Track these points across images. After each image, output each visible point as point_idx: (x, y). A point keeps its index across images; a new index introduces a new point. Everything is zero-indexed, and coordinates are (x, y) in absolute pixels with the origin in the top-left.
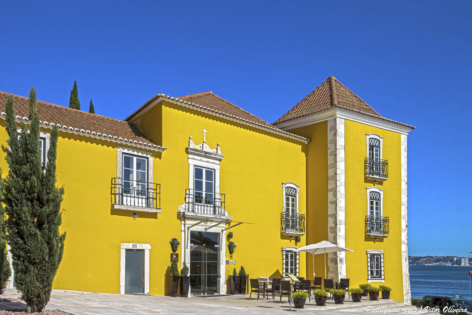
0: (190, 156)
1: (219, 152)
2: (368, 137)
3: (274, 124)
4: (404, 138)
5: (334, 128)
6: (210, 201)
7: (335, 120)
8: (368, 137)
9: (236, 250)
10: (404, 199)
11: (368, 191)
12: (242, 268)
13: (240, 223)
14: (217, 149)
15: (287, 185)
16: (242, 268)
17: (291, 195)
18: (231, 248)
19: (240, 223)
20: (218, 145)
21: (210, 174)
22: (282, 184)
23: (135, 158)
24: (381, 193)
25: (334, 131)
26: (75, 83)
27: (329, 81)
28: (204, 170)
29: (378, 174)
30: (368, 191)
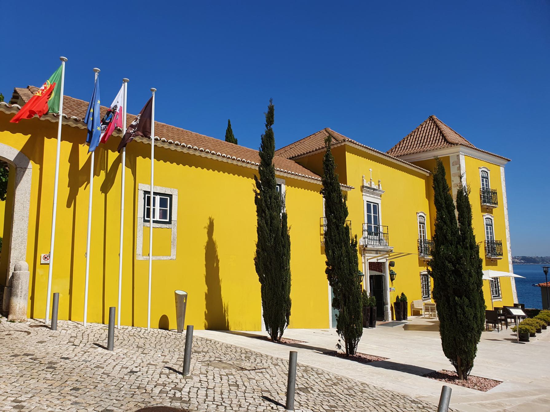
0: (364, 194)
1: (381, 188)
2: (480, 170)
3: (397, 156)
4: (502, 169)
5: (458, 163)
6: (377, 233)
7: (458, 156)
8: (480, 170)
9: (396, 278)
10: (507, 224)
11: (485, 217)
12: (403, 294)
13: (409, 254)
14: (379, 185)
15: (420, 214)
16: (403, 294)
17: (255, 191)
18: (392, 275)
19: (409, 254)
20: (379, 181)
21: (376, 207)
22: (417, 213)
23: (372, 204)
24: (492, 218)
25: (458, 166)
26: (229, 122)
27: (431, 119)
28: (372, 204)
29: (489, 202)
30: (485, 217)
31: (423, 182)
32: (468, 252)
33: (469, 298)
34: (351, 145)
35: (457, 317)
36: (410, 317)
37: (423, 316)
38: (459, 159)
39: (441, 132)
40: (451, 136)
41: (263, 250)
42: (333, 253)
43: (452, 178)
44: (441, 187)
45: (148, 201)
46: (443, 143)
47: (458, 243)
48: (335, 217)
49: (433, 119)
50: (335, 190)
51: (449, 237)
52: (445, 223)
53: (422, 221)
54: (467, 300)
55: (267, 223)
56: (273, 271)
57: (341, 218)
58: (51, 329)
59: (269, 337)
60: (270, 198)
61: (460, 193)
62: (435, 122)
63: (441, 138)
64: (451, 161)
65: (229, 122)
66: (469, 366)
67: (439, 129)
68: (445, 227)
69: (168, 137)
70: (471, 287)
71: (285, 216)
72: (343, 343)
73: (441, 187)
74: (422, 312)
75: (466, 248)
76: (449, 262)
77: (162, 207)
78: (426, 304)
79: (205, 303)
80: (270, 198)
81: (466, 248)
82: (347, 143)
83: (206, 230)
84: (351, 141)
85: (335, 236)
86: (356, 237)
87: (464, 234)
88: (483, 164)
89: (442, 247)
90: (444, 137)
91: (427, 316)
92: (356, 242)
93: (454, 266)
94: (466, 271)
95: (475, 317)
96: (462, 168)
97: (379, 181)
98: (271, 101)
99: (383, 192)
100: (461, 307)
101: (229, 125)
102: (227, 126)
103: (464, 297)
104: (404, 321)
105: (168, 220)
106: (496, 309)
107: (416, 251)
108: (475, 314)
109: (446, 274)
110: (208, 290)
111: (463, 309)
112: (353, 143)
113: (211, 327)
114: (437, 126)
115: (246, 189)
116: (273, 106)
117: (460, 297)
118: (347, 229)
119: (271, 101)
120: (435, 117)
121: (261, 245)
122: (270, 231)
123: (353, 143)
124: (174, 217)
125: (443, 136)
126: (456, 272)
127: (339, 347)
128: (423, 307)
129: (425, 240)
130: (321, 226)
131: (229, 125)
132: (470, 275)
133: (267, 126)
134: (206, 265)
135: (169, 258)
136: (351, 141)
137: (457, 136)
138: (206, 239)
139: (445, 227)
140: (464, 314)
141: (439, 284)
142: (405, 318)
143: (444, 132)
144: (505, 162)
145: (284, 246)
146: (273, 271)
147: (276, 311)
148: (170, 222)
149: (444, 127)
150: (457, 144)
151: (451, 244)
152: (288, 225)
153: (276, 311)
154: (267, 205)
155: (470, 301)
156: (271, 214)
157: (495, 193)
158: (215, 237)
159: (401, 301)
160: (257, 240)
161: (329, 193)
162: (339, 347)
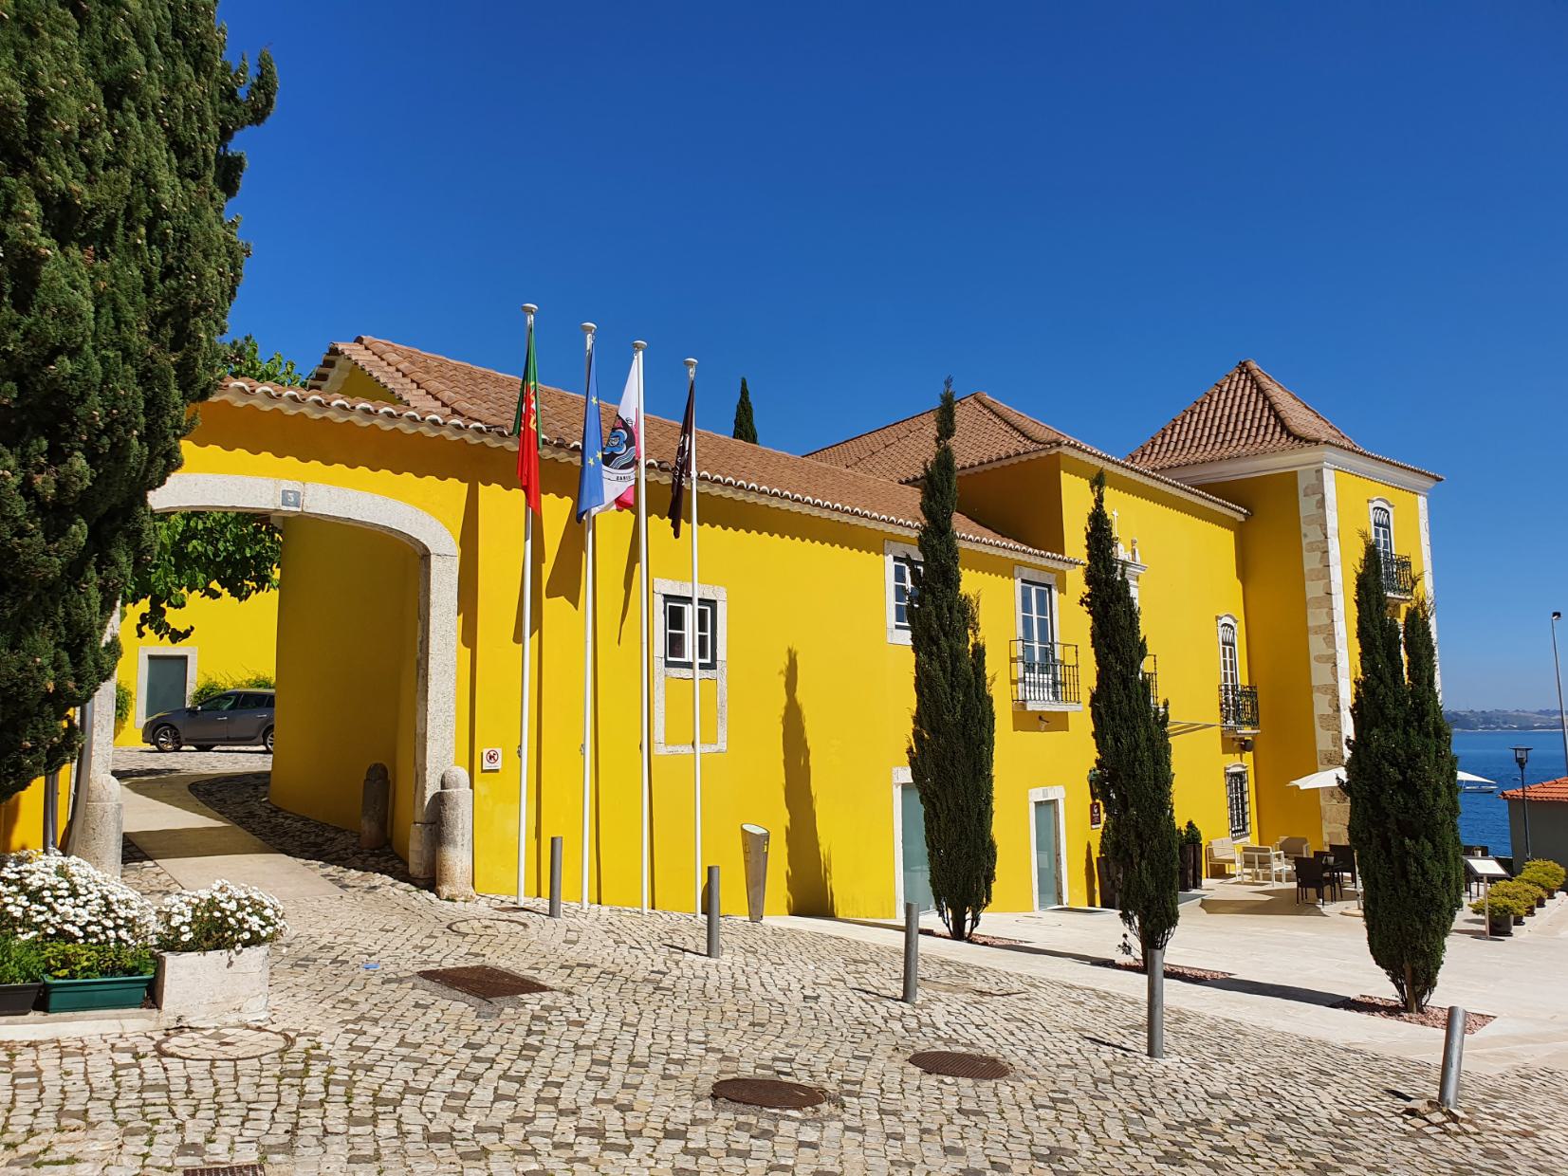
2: (1372, 506)
4: (1422, 501)
5: (1319, 489)
7: (1319, 471)
8: (1372, 506)
12: (1190, 825)
20: (1133, 542)
22: (1218, 618)
26: (744, 384)
27: (1243, 368)
31: (1229, 536)
32: (1432, 743)
33: (1433, 842)
34: (1074, 453)
35: (1408, 882)
36: (1206, 882)
37: (1238, 879)
38: (1321, 480)
39: (1271, 407)
40: (1299, 417)
41: (932, 731)
42: (1117, 740)
43: (1304, 528)
44: (1374, 602)
45: (675, 619)
46: (1277, 436)
47: (1408, 723)
48: (1120, 660)
49: (1248, 371)
50: (1119, 599)
51: (1391, 710)
52: (1381, 680)
53: (1229, 637)
54: (1429, 846)
55: (944, 671)
56: (960, 779)
57: (1133, 662)
58: (551, 915)
59: (945, 931)
60: (950, 609)
61: (1412, 615)
62: (1253, 379)
63: (1272, 421)
64: (1302, 485)
65: (744, 384)
66: (1430, 983)
67: (1266, 398)
68: (1382, 690)
69: (760, 483)
70: (1439, 816)
71: (979, 652)
72: (1136, 945)
73: (1374, 602)
74: (1235, 869)
75: (1427, 735)
76: (1392, 765)
77: (686, 629)
78: (1245, 849)
79: (786, 850)
80: (950, 609)
81: (1427, 735)
82: (1064, 450)
83: (783, 679)
84: (1074, 446)
85: (1120, 702)
86: (1166, 706)
87: (1422, 704)
88: (1377, 490)
89: (1375, 731)
90: (1279, 419)
91: (1247, 878)
92: (1166, 717)
93: (1403, 773)
94: (1428, 784)
95: (1446, 880)
96: (1328, 503)
97: (1133, 542)
98: (948, 383)
99: (1144, 568)
100: (1416, 860)
101: (744, 392)
102: (739, 396)
103: (1422, 838)
104: (1194, 891)
105: (708, 661)
106: (1319, 855)
107: (1216, 718)
108: (1447, 874)
109: (1382, 790)
110: (791, 821)
111: (1420, 864)
112: (1079, 449)
113: (798, 910)
114: (1260, 390)
115: (874, 584)
116: (952, 395)
117: (1415, 837)
118: (1146, 686)
119: (948, 383)
120: (1253, 365)
121: (927, 717)
122: (952, 686)
123: (1079, 449)
124: (721, 655)
125: (1277, 416)
126: (1407, 786)
127: (1126, 949)
128: (1238, 856)
129: (1234, 688)
130: (1013, 660)
131: (744, 392)
132: (1437, 794)
133: (937, 440)
134: (786, 763)
135: (715, 748)
136: (1074, 446)
137: (1311, 417)
138: (784, 700)
139: (1382, 690)
140: (1425, 873)
141: (1366, 810)
142: (1197, 885)
143: (1279, 407)
144: (1430, 484)
145: (982, 722)
146: (960, 779)
147: (958, 866)
148: (712, 666)
149: (1276, 393)
150: (1317, 442)
151: (1395, 727)
152: (989, 672)
153: (958, 866)
154: (941, 626)
155: (1435, 846)
156: (951, 647)
157: (1405, 564)
158: (799, 695)
159: (1188, 841)
160: (914, 707)
161: (1105, 605)
162: (1126, 949)
